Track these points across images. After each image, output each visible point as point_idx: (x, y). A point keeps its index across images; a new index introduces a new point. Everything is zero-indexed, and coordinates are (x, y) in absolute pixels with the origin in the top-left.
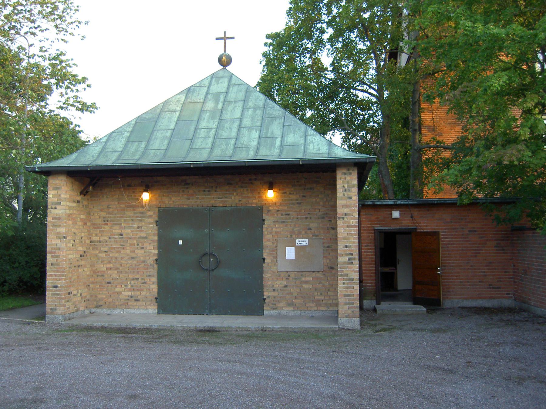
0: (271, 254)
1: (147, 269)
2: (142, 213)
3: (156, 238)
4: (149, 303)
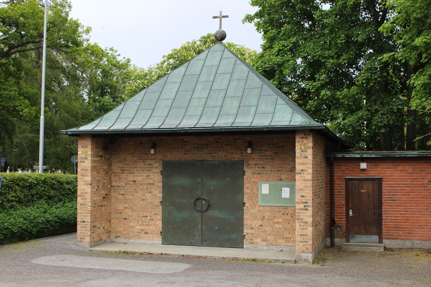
0: (250, 199)
2: (150, 165)
3: (161, 184)
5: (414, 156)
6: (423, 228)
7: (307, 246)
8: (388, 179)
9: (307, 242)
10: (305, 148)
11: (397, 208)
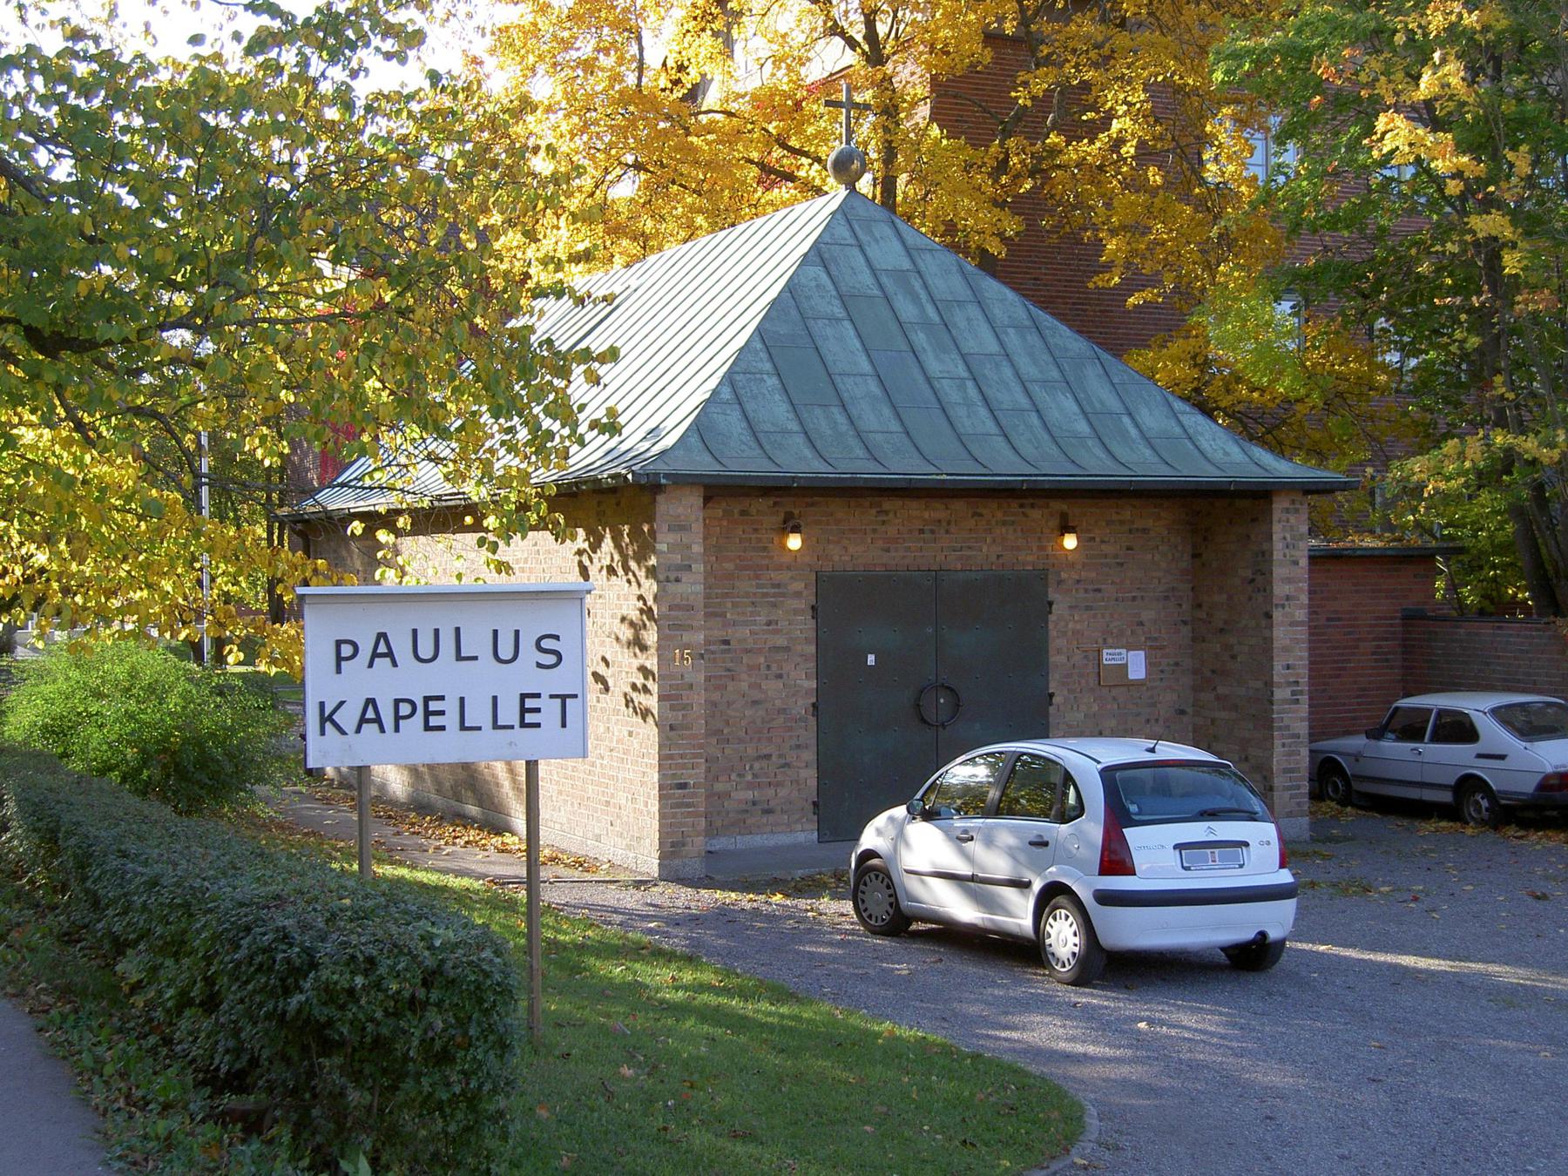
1: (790, 729)
2: (778, 586)
3: (812, 649)
4: (797, 817)
9: (1298, 787)
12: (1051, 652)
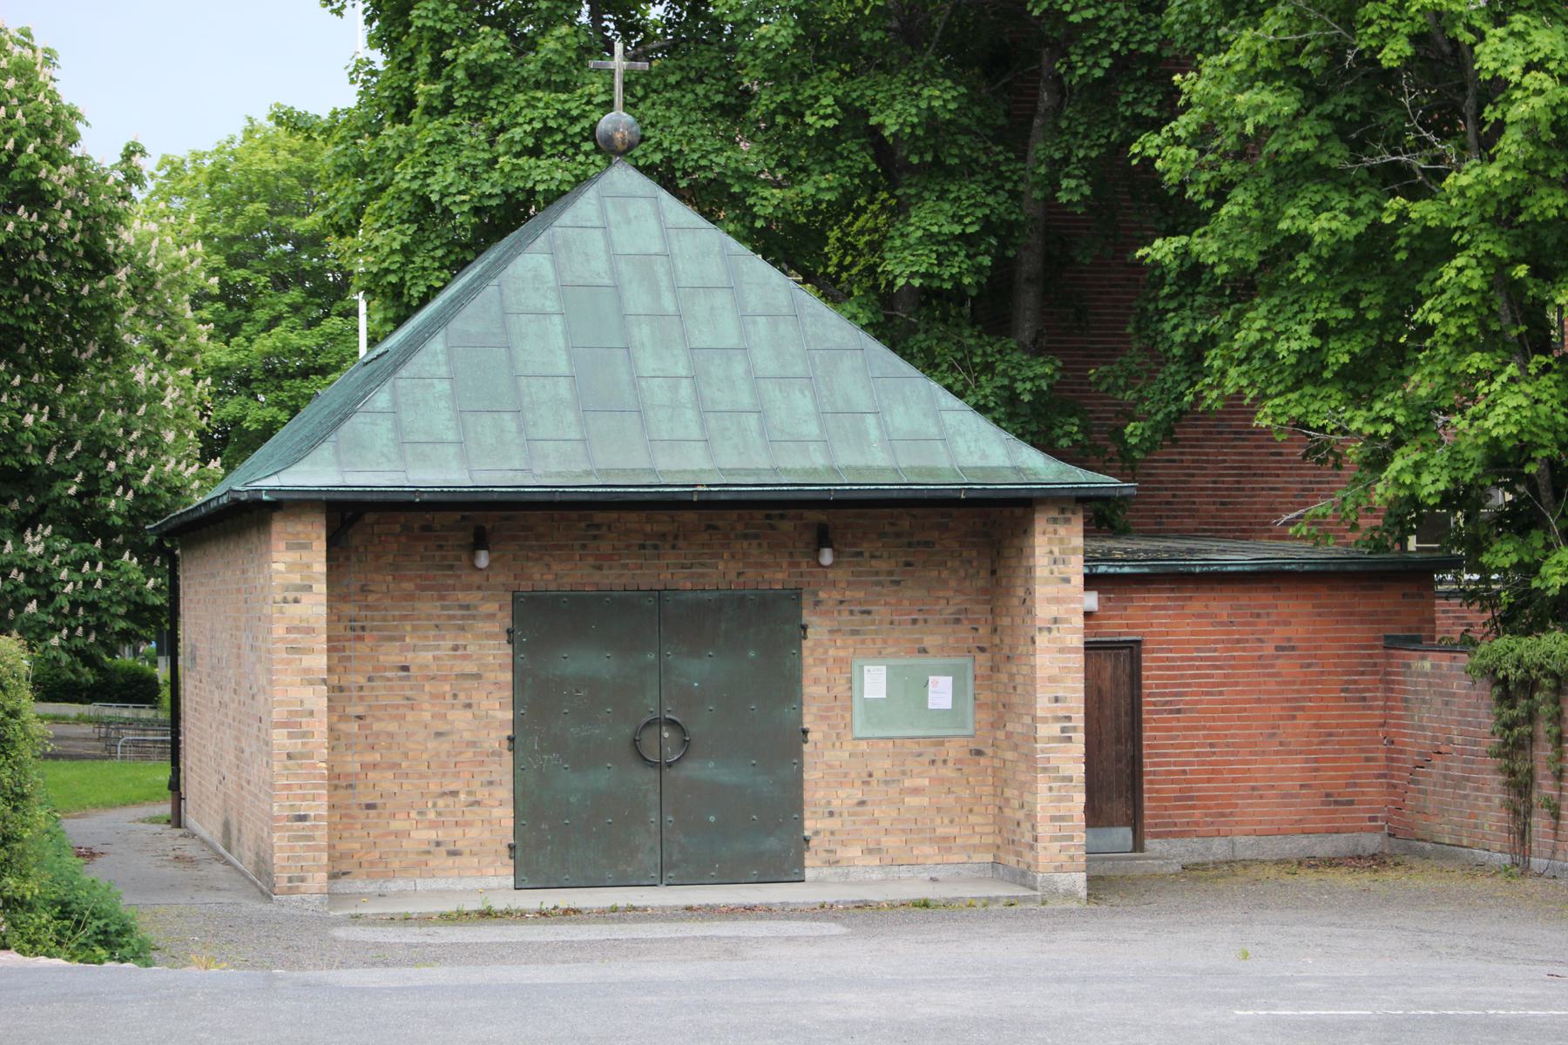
0: (823, 718)
2: (467, 607)
3: (507, 676)
5: (1247, 568)
6: (1261, 797)
7: (1072, 851)
8: (1160, 643)
9: (1071, 838)
10: (1062, 552)
11: (1185, 737)
12: (805, 683)
